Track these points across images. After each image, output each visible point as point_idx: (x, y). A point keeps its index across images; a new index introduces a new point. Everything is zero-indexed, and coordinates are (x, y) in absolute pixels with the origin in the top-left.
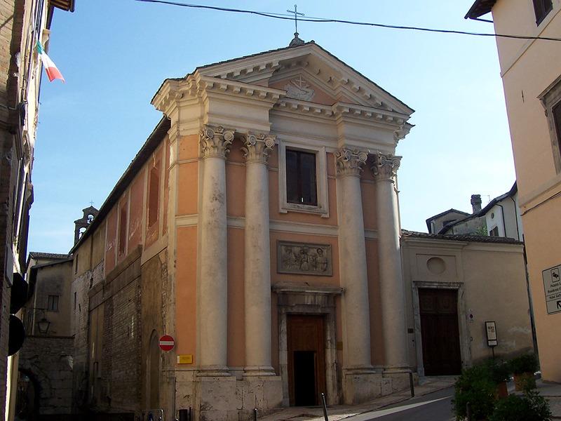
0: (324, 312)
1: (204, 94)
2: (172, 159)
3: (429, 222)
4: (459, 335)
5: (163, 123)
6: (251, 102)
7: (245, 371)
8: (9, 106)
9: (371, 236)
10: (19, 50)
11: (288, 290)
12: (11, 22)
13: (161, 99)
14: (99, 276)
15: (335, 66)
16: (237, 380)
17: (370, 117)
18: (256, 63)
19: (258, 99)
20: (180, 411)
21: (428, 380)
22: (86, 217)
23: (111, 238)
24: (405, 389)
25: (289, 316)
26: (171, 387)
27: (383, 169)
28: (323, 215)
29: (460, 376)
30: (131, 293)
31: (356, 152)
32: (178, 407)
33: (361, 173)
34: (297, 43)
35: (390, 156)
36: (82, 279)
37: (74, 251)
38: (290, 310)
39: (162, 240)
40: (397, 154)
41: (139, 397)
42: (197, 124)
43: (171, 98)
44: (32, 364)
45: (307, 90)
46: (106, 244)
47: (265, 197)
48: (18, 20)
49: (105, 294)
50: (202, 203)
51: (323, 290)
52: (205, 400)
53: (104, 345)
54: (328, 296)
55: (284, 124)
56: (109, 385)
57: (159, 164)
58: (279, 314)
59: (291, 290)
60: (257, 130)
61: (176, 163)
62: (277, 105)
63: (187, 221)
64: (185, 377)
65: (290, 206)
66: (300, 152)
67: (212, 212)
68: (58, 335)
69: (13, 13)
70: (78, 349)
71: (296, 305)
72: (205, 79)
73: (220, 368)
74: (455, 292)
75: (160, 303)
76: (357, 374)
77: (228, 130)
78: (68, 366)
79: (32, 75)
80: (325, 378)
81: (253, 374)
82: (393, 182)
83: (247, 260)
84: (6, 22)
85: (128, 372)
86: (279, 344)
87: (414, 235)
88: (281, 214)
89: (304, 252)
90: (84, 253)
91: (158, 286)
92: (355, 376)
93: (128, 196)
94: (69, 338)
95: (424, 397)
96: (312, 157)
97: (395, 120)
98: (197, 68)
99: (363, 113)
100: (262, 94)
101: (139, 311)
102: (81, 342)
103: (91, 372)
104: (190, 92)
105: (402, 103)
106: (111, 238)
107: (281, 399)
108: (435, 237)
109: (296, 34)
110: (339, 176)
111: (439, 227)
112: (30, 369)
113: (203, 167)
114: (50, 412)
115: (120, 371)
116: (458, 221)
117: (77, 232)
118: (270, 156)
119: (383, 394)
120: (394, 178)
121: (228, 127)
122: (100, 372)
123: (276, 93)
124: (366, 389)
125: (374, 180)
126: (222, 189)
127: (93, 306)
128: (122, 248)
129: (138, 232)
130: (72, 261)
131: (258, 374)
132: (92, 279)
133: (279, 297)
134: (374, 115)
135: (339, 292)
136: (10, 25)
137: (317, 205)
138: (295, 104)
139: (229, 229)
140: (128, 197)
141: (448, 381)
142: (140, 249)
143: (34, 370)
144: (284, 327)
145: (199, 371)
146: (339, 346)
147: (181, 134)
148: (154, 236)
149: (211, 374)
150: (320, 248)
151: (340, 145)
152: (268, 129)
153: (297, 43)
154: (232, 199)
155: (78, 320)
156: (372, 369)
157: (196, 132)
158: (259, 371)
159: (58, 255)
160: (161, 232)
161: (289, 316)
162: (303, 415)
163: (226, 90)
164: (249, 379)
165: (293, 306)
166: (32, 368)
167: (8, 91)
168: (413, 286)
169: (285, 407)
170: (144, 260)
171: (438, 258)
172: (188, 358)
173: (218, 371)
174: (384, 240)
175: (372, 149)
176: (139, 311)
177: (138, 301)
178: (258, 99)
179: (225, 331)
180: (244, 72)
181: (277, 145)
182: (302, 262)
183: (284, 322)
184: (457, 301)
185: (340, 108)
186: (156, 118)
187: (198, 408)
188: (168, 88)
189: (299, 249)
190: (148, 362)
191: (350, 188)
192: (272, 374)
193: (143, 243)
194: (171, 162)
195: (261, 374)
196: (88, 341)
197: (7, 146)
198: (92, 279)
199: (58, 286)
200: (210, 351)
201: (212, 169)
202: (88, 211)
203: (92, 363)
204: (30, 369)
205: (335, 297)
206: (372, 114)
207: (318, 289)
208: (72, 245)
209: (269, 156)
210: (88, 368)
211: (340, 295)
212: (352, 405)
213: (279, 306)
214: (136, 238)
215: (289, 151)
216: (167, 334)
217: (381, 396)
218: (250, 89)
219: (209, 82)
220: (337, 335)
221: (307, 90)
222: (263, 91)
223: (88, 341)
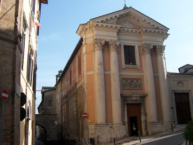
0: (140, 103)
1: (94, 28)
2: (84, 51)
3: (179, 69)
4: (190, 109)
5: (81, 40)
6: (105, 30)
7: (112, 124)
8: (15, 35)
9: (156, 75)
10: (18, 16)
11: (127, 95)
12: (15, 6)
13: (79, 31)
14: (64, 93)
15: (139, 15)
16: (110, 127)
17: (153, 32)
18: (111, 16)
19: (112, 29)
20: (90, 139)
21: (179, 126)
22: (59, 74)
23: (67, 81)
24: (170, 129)
25: (127, 104)
26: (87, 130)
27: (159, 51)
28: (138, 68)
29: (187, 124)
30: (74, 99)
31: (149, 45)
32: (90, 137)
33: (151, 52)
34: (125, 8)
35: (161, 46)
36: (59, 95)
37: (56, 85)
38: (128, 102)
39: (83, 79)
40: (164, 45)
41: (78, 134)
42: (92, 39)
43: (82, 31)
44: (43, 124)
45: (130, 24)
46: (66, 83)
47: (117, 63)
48: (17, 5)
49: (66, 99)
50: (95, 66)
51: (139, 95)
52: (98, 135)
53: (66, 117)
54: (141, 97)
55: (122, 37)
56: (69, 130)
57: (81, 54)
58: (124, 104)
59: (128, 95)
60: (113, 40)
61: (86, 53)
62: (119, 30)
63: (90, 73)
64: (92, 127)
65: (126, 66)
66: (129, 47)
67: (99, 69)
68: (52, 114)
69: (15, 3)
70: (59, 118)
71: (130, 100)
72: (94, 23)
73: (103, 124)
74: (188, 94)
75: (83, 102)
76: (152, 124)
77: (103, 40)
78: (55, 124)
79: (32, 26)
80: (141, 126)
81: (115, 125)
82: (163, 55)
83: (112, 85)
84: (13, 6)
85: (74, 125)
86: (124, 114)
87: (172, 74)
88: (123, 68)
89: (132, 82)
90: (59, 86)
91: (82, 96)
92: (152, 125)
93: (72, 66)
94: (55, 115)
95: (177, 132)
96: (133, 48)
97: (162, 33)
98: (90, 19)
99: (150, 31)
100: (104, 26)
101: (77, 105)
102: (60, 116)
103: (63, 126)
104: (89, 28)
105: (162, 25)
106: (67, 81)
107: (125, 134)
108: (182, 74)
109: (125, 5)
110: (143, 54)
111: (183, 71)
112: (43, 126)
113: (95, 54)
114: (50, 139)
115: (72, 125)
116: (190, 68)
117: (57, 79)
118: (118, 48)
119: (162, 131)
120: (163, 53)
121: (102, 39)
122: (66, 126)
123: (119, 26)
124: (156, 130)
125: (156, 55)
126: (102, 61)
127: (63, 104)
128: (71, 84)
129: (75, 78)
130: (56, 89)
131: (117, 125)
132: (62, 95)
133: (124, 98)
134: (154, 31)
135: (145, 95)
136: (14, 7)
137: (136, 65)
138: (126, 30)
139: (105, 75)
140: (72, 66)
141: (183, 127)
142: (76, 84)
143: (44, 126)
144: (126, 108)
145: (96, 125)
146: (146, 115)
147: (87, 43)
148: (80, 79)
149: (100, 126)
150: (138, 80)
151: (143, 43)
152: (117, 39)
153: (125, 8)
154: (105, 64)
155: (58, 108)
156: (158, 122)
157: (92, 42)
158: (117, 124)
159: (51, 87)
160: (82, 77)
161: (127, 104)
162: (133, 139)
163: (111, 27)
164: (114, 127)
165: (129, 101)
166: (43, 126)
167: (14, 30)
168: (172, 92)
169: (127, 137)
170: (78, 86)
171: (181, 82)
172: (92, 120)
173: (103, 124)
174: (160, 75)
175: (155, 44)
176: (77, 105)
177: (76, 101)
178: (112, 29)
179: (105, 110)
180: (107, 20)
181: (120, 44)
182: (131, 85)
183: (126, 106)
184: (189, 97)
185: (142, 30)
186: (79, 38)
187: (96, 138)
188: (81, 27)
189: (130, 81)
190: (80, 122)
191: (147, 58)
192: (122, 125)
193: (77, 81)
194: (84, 53)
195: (118, 125)
196: (62, 116)
197: (15, 49)
198: (62, 95)
199: (51, 98)
200: (100, 118)
201: (98, 54)
202: (60, 72)
203: (63, 123)
204: (43, 126)
205: (143, 97)
206: (154, 31)
207: (138, 95)
208: (55, 83)
209: (118, 48)
210: (62, 125)
211: (145, 96)
212: (151, 135)
213: (124, 101)
214: (75, 80)
215: (125, 47)
216: (85, 112)
217: (162, 132)
218: (109, 25)
219: (95, 24)
220: (145, 110)
221: (130, 24)
222: (114, 26)
223: (62, 116)
